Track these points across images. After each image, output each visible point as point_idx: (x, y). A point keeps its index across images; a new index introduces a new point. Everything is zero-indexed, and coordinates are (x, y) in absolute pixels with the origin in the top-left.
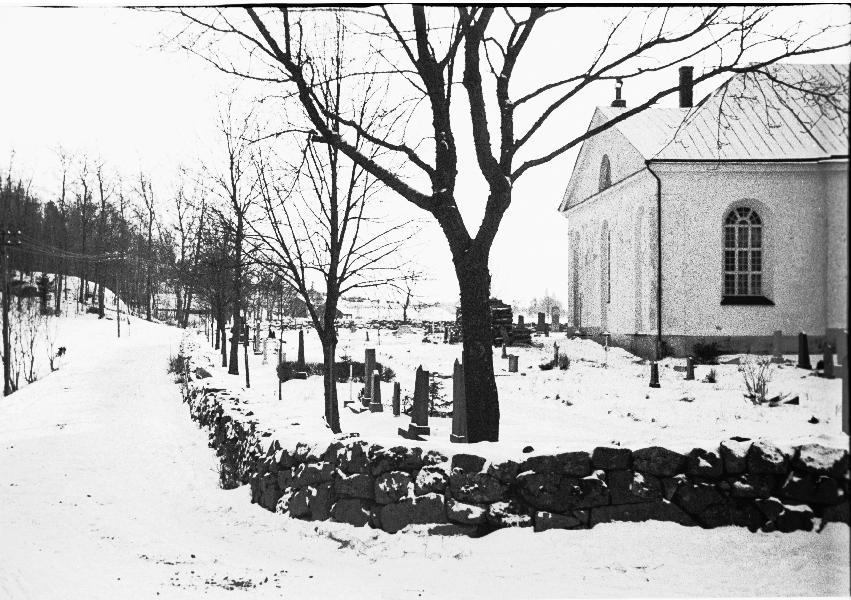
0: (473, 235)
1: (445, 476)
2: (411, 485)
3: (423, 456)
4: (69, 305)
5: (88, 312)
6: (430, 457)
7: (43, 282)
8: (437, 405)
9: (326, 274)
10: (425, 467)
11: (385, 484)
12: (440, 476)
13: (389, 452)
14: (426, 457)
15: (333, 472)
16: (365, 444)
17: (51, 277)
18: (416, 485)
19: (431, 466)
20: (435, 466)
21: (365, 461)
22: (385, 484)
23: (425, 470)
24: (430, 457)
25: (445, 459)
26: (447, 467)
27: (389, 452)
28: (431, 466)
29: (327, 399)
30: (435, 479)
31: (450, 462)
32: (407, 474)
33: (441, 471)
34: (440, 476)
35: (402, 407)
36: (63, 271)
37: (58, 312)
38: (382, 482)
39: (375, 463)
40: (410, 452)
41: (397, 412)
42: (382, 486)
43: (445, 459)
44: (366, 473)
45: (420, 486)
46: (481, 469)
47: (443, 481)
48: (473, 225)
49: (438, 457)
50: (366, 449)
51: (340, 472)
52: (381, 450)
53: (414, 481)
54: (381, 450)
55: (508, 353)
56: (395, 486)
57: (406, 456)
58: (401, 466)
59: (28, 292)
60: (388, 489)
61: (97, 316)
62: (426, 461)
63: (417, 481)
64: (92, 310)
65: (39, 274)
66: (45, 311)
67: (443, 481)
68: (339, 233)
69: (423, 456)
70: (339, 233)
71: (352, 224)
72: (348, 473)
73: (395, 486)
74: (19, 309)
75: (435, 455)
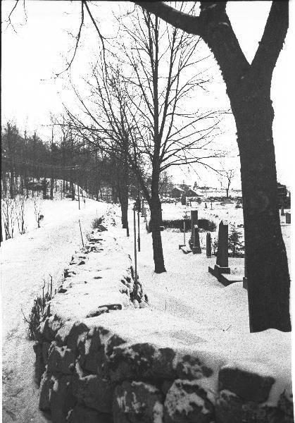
0: (250, 64)
1: (207, 401)
2: (158, 407)
3: (175, 362)
4: (57, 195)
5: (67, 197)
6: (186, 365)
7: (44, 182)
8: (237, 248)
9: (151, 155)
10: (179, 381)
11: (123, 398)
12: (200, 402)
13: (130, 351)
14: (180, 365)
15: (72, 365)
16: (105, 332)
17: (49, 180)
18: (165, 409)
19: (186, 382)
20: (192, 383)
21: (102, 360)
22: (123, 398)
23: (178, 385)
24: (186, 365)
25: (208, 372)
26: (208, 384)
27: (130, 351)
28: (186, 382)
29: (154, 248)
30: (193, 404)
31: (216, 377)
32: (152, 389)
33: (202, 393)
34: (200, 402)
35: (212, 251)
36: (54, 177)
37: (52, 198)
38: (121, 395)
39: (113, 365)
40: (157, 355)
41: (209, 255)
42: (120, 401)
43: (208, 372)
44: (103, 377)
45: (171, 413)
46: (266, 398)
47: (205, 411)
48: (249, 39)
49: (197, 367)
50: (105, 341)
51: (77, 366)
52: (121, 347)
53: (162, 402)
54: (121, 347)
55: (285, 212)
56: (136, 406)
57: (151, 360)
58: (146, 374)
59: (37, 188)
60: (127, 408)
61: (71, 199)
62: (179, 373)
63: (166, 403)
64: (68, 196)
65: (42, 179)
66: (45, 197)
67: (205, 411)
68: (159, 129)
69: (175, 362)
70: (159, 129)
71: (168, 118)
72: (86, 372)
73: (136, 406)
74: (33, 196)
75: (193, 364)
